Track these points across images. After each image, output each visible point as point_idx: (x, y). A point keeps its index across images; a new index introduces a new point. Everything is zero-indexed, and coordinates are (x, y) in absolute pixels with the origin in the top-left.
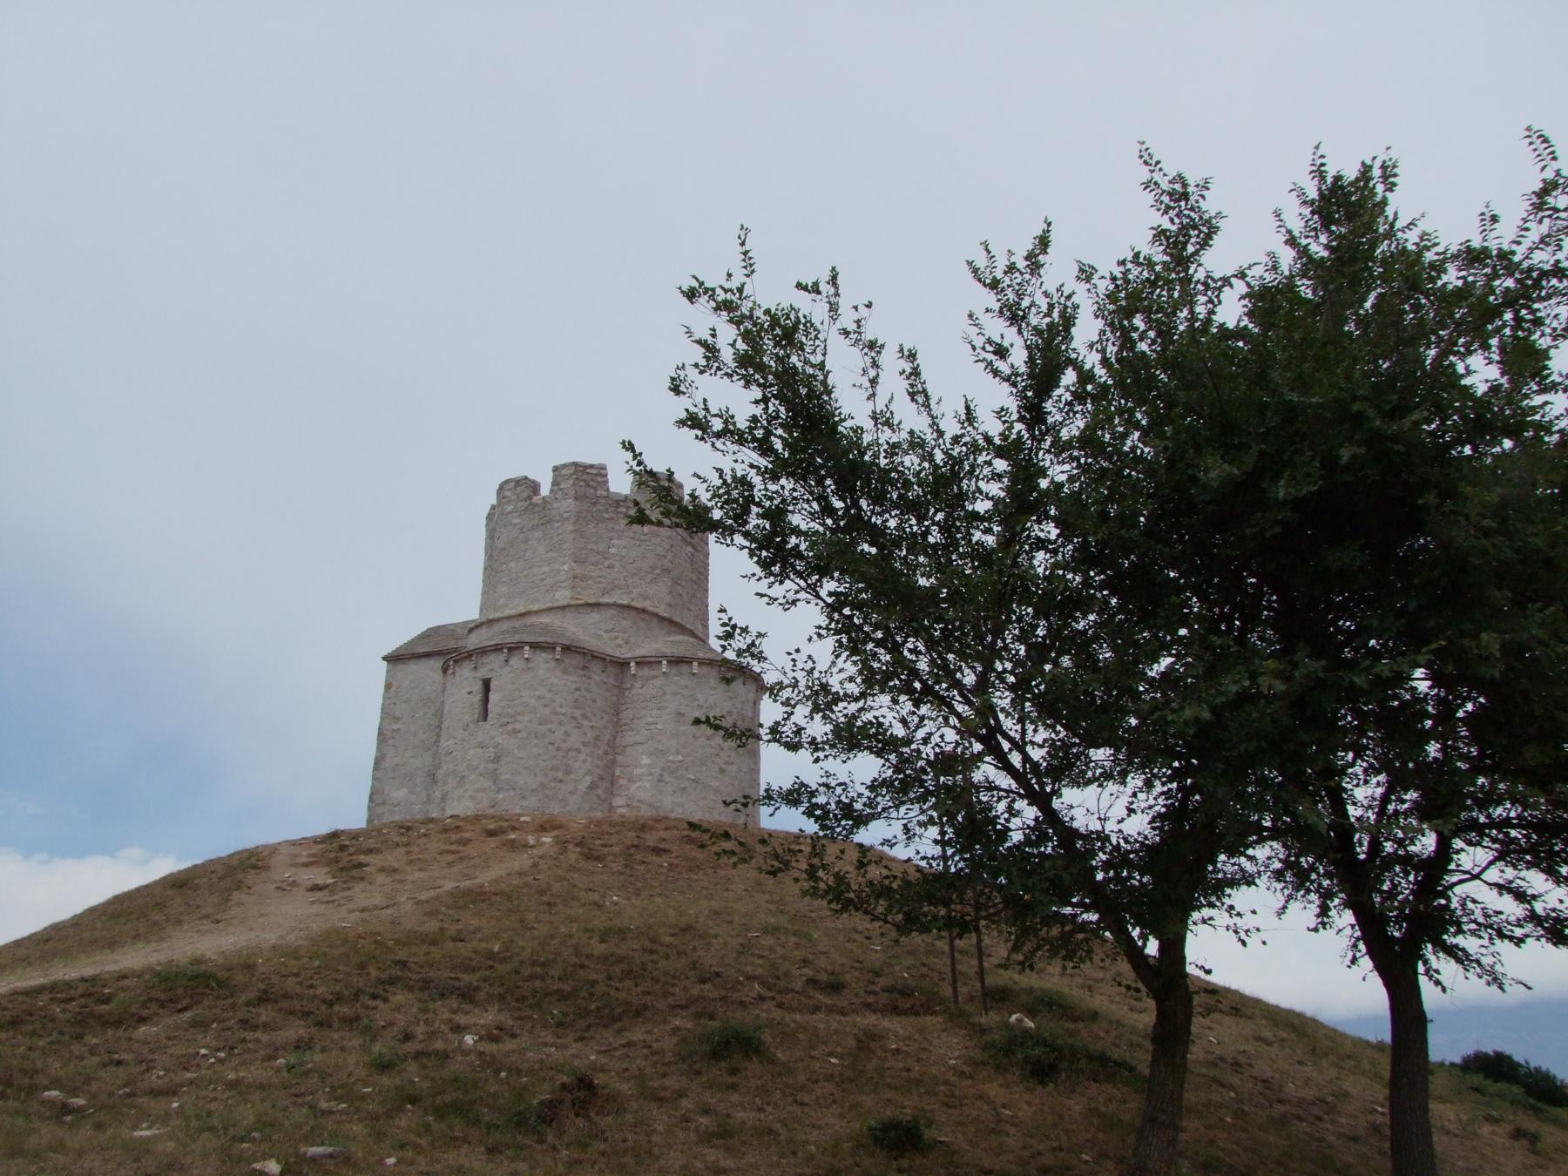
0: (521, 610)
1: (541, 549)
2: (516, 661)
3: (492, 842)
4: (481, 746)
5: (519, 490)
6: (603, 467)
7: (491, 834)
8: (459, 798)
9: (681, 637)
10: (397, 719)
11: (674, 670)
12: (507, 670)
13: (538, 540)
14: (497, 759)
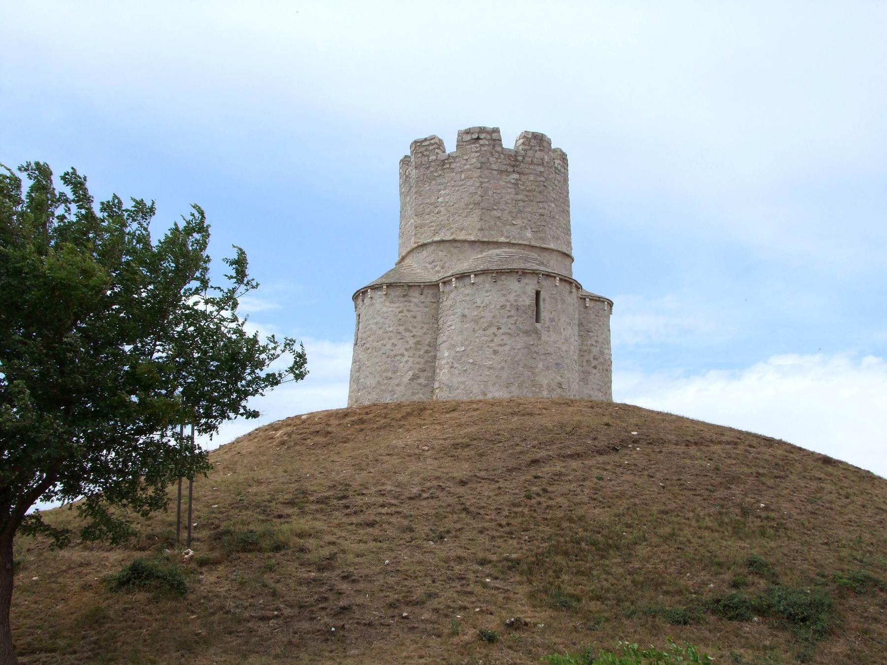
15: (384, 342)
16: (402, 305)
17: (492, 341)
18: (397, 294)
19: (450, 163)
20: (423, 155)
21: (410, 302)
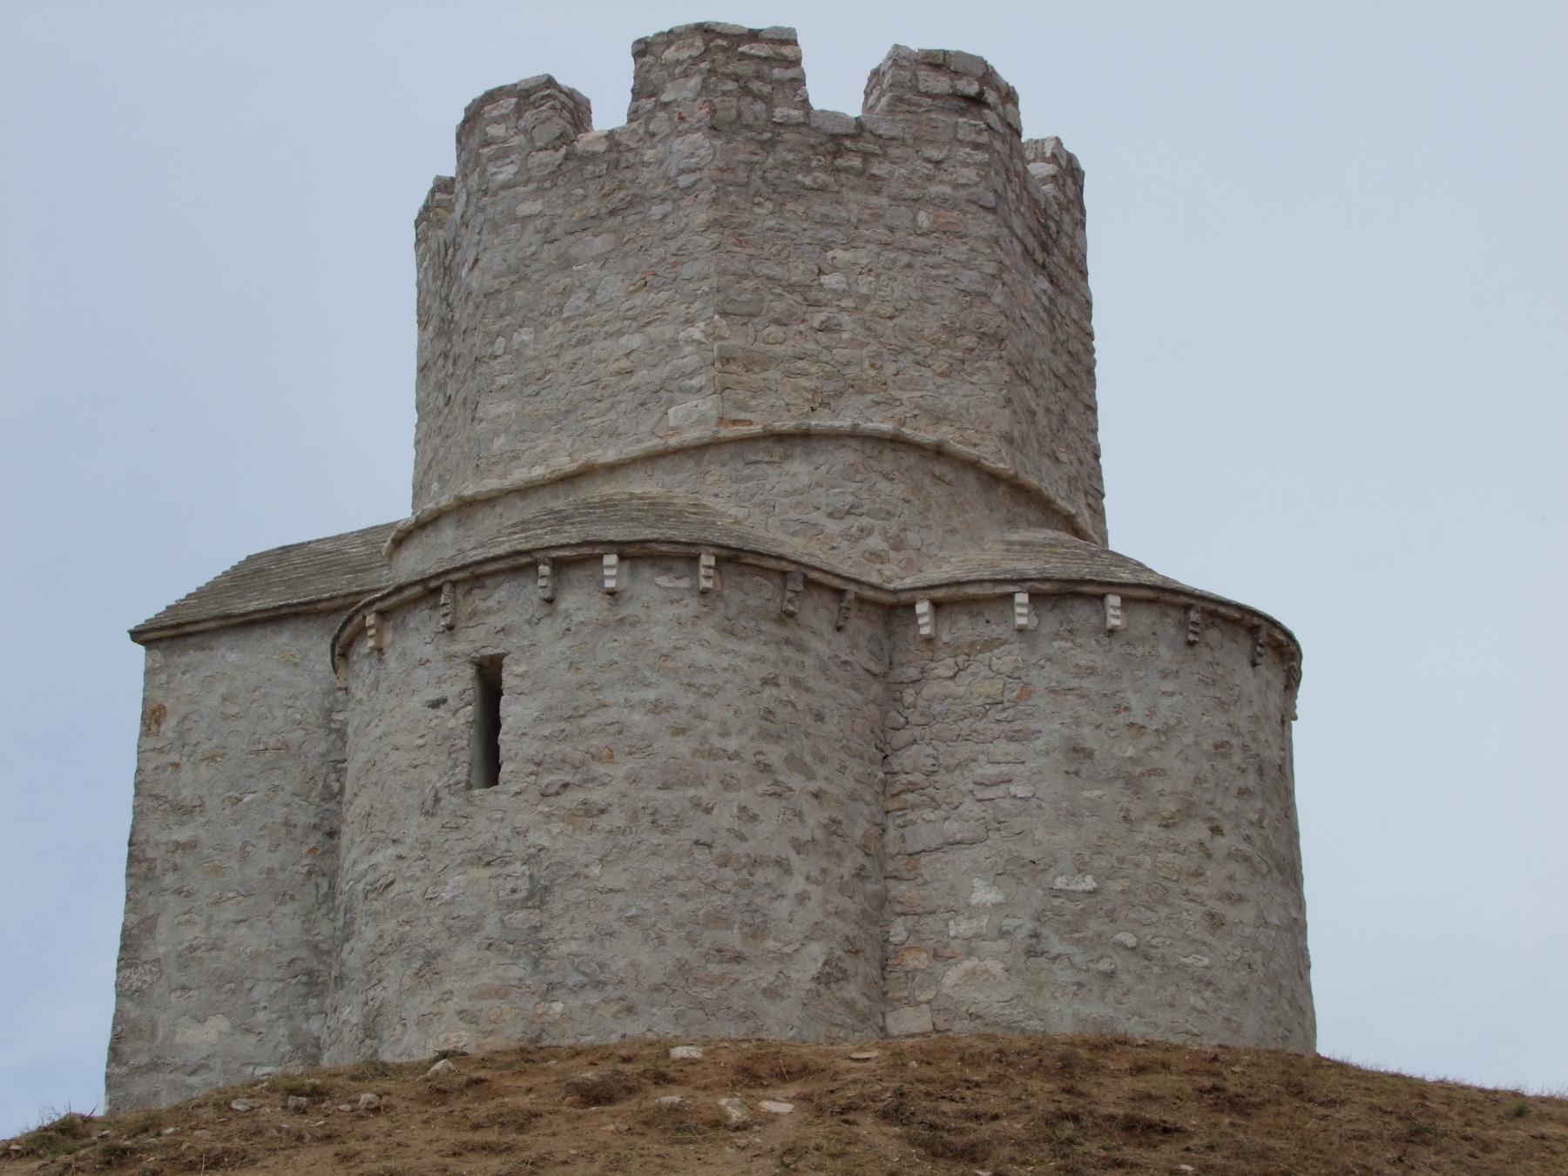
0: (564, 463)
1: (613, 286)
2: (579, 602)
3: (606, 1124)
4: (485, 858)
5: (539, 110)
6: (787, 39)
7: (594, 1096)
8: (424, 1020)
9: (1047, 534)
10: (184, 812)
11: (1051, 623)
12: (547, 630)
13: (603, 260)
14: (538, 895)
15: (704, 794)
16: (770, 652)
17: (1197, 874)
18: (753, 601)
19: (866, 156)
20: (746, 91)
21: (802, 648)
